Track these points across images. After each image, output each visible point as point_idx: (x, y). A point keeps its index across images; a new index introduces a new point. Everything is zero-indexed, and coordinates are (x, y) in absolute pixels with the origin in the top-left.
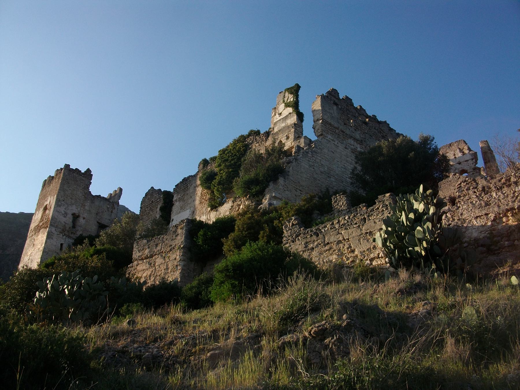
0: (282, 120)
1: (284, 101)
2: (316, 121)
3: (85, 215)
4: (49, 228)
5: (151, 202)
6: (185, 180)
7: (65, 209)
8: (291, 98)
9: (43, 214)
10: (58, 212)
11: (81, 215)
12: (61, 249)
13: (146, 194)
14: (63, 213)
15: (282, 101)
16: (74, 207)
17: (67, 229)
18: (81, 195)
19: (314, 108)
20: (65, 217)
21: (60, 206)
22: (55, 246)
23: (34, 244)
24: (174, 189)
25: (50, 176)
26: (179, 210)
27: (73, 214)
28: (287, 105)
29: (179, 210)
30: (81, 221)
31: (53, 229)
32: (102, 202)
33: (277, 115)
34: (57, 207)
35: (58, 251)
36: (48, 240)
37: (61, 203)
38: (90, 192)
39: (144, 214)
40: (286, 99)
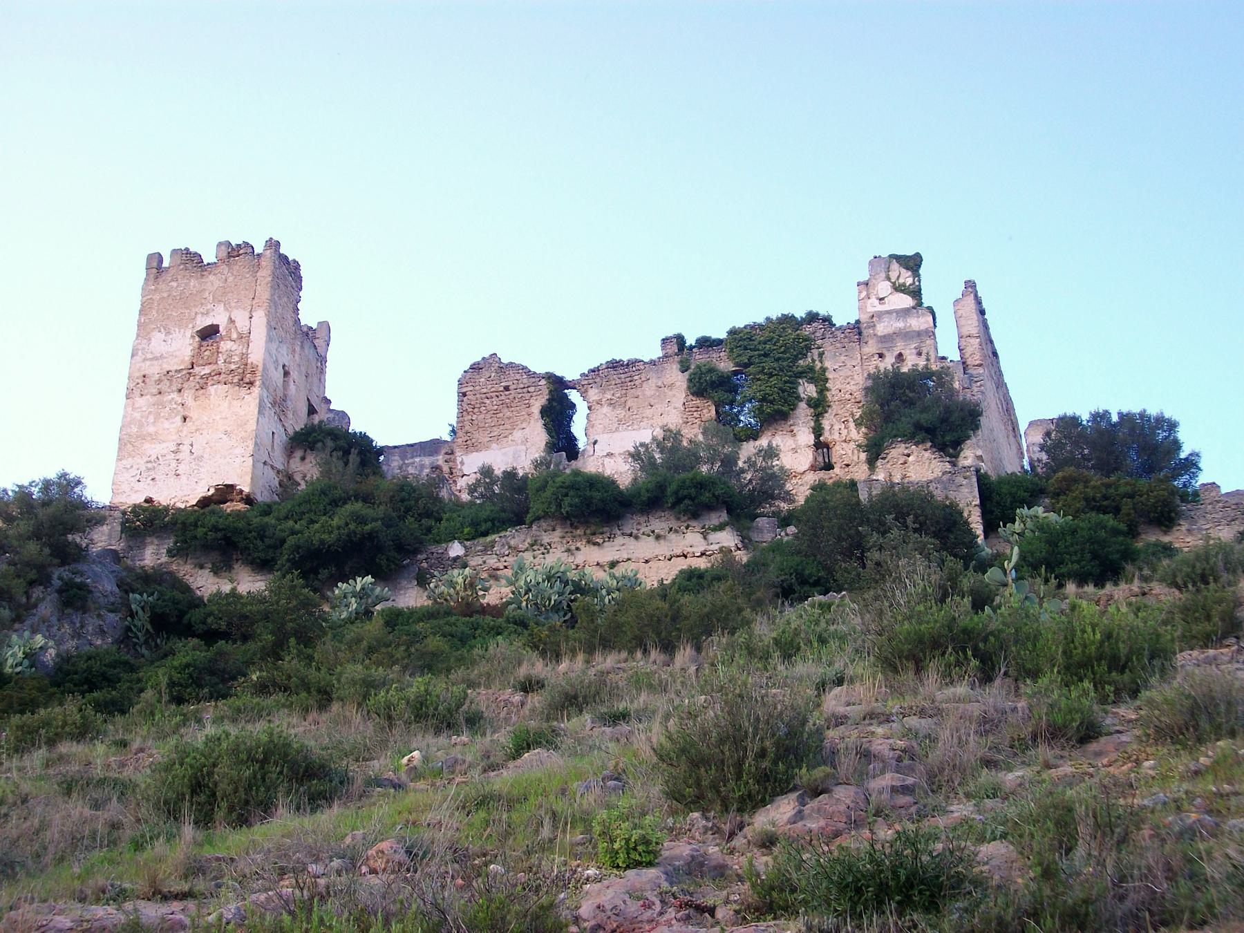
1: (888, 279)
5: (502, 389)
6: (614, 365)
8: (907, 278)
13: (476, 368)
15: (883, 275)
26: (616, 425)
28: (899, 288)
29: (616, 425)
33: (874, 301)
40: (893, 276)
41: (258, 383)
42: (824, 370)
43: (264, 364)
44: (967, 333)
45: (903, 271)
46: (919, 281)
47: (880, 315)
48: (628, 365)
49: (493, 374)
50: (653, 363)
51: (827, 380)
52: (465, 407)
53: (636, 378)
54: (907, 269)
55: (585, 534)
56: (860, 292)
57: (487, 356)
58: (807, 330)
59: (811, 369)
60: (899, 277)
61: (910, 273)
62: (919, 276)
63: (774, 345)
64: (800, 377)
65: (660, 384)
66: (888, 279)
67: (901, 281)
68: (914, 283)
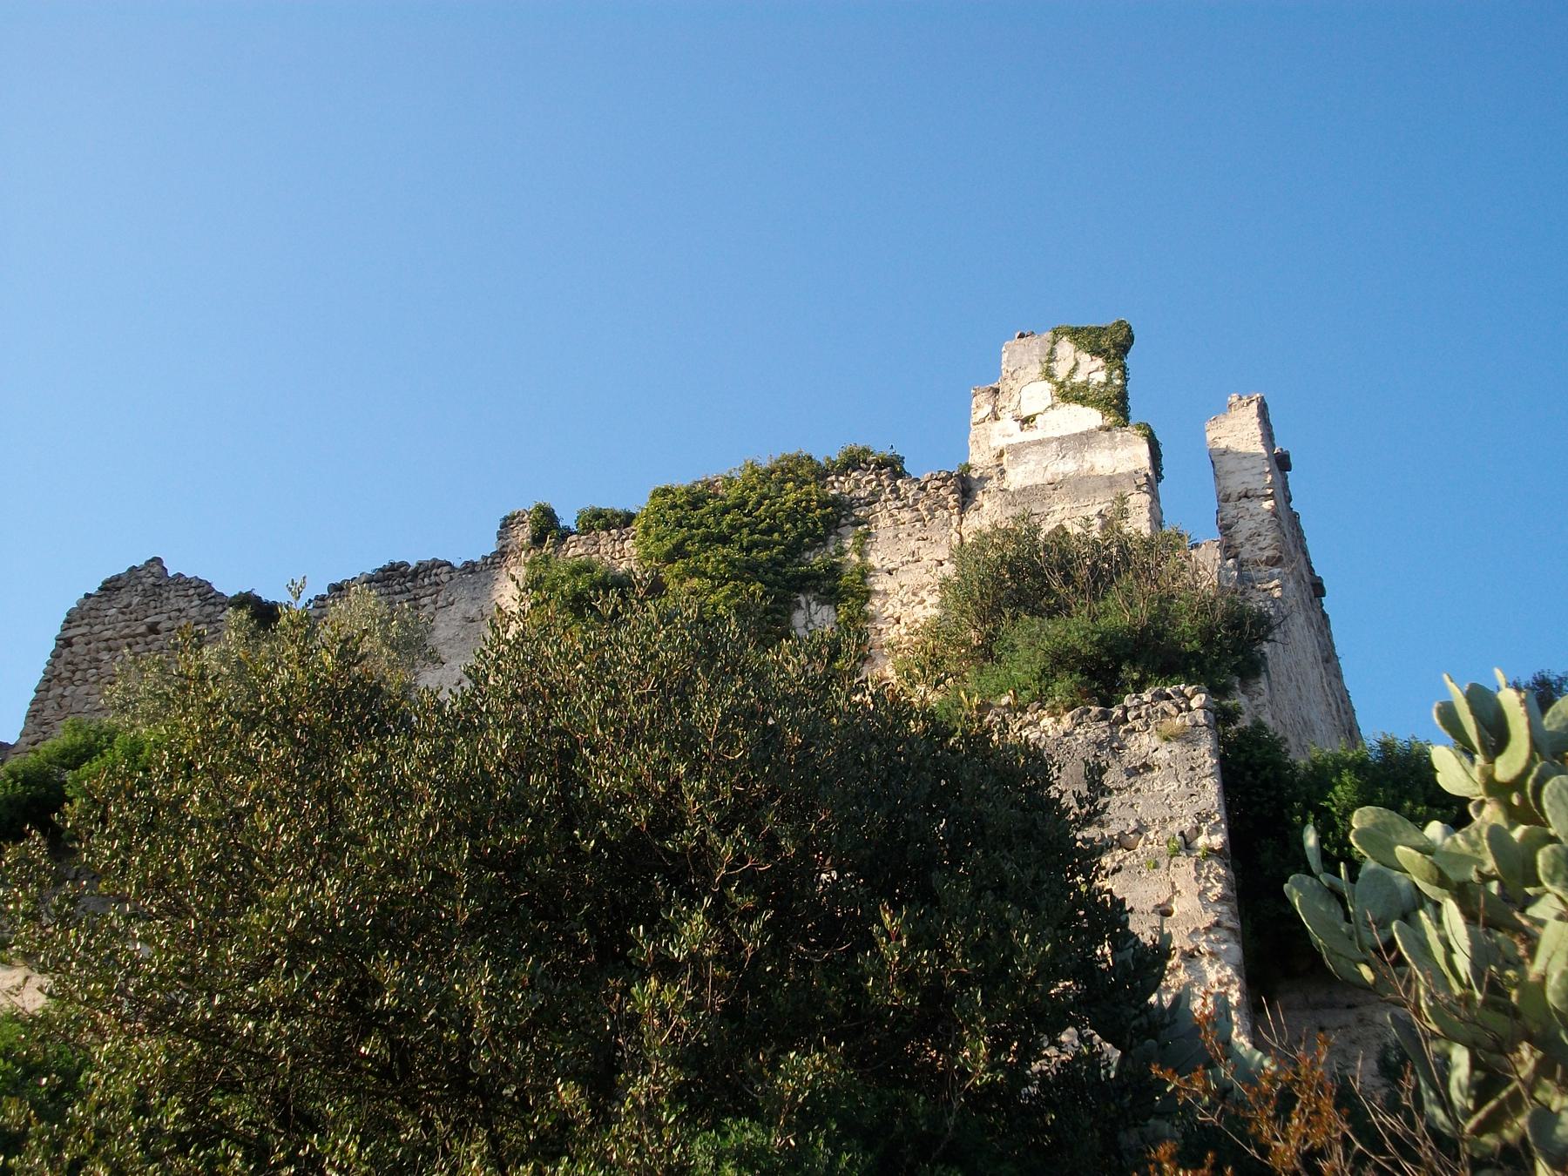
0: (1055, 445)
2: (1235, 496)
5: (142, 629)
8: (1093, 371)
13: (111, 587)
15: (1036, 370)
19: (1222, 445)
24: (88, 596)
25: (157, 561)
28: (1071, 394)
33: (1008, 424)
36: (372, 600)
38: (180, 575)
39: (78, 675)
40: (1061, 371)
42: (865, 572)
44: (1241, 489)
45: (1085, 358)
46: (1124, 376)
47: (1017, 450)
48: (415, 573)
49: (136, 600)
50: (470, 567)
51: (867, 595)
52: (60, 667)
53: (425, 600)
54: (1096, 352)
55: (255, 1089)
57: (140, 563)
58: (840, 486)
59: (834, 571)
60: (1074, 370)
61: (1100, 362)
62: (1124, 370)
63: (749, 514)
64: (800, 590)
65: (473, 612)
66: (1049, 375)
67: (1079, 378)
68: (1109, 381)
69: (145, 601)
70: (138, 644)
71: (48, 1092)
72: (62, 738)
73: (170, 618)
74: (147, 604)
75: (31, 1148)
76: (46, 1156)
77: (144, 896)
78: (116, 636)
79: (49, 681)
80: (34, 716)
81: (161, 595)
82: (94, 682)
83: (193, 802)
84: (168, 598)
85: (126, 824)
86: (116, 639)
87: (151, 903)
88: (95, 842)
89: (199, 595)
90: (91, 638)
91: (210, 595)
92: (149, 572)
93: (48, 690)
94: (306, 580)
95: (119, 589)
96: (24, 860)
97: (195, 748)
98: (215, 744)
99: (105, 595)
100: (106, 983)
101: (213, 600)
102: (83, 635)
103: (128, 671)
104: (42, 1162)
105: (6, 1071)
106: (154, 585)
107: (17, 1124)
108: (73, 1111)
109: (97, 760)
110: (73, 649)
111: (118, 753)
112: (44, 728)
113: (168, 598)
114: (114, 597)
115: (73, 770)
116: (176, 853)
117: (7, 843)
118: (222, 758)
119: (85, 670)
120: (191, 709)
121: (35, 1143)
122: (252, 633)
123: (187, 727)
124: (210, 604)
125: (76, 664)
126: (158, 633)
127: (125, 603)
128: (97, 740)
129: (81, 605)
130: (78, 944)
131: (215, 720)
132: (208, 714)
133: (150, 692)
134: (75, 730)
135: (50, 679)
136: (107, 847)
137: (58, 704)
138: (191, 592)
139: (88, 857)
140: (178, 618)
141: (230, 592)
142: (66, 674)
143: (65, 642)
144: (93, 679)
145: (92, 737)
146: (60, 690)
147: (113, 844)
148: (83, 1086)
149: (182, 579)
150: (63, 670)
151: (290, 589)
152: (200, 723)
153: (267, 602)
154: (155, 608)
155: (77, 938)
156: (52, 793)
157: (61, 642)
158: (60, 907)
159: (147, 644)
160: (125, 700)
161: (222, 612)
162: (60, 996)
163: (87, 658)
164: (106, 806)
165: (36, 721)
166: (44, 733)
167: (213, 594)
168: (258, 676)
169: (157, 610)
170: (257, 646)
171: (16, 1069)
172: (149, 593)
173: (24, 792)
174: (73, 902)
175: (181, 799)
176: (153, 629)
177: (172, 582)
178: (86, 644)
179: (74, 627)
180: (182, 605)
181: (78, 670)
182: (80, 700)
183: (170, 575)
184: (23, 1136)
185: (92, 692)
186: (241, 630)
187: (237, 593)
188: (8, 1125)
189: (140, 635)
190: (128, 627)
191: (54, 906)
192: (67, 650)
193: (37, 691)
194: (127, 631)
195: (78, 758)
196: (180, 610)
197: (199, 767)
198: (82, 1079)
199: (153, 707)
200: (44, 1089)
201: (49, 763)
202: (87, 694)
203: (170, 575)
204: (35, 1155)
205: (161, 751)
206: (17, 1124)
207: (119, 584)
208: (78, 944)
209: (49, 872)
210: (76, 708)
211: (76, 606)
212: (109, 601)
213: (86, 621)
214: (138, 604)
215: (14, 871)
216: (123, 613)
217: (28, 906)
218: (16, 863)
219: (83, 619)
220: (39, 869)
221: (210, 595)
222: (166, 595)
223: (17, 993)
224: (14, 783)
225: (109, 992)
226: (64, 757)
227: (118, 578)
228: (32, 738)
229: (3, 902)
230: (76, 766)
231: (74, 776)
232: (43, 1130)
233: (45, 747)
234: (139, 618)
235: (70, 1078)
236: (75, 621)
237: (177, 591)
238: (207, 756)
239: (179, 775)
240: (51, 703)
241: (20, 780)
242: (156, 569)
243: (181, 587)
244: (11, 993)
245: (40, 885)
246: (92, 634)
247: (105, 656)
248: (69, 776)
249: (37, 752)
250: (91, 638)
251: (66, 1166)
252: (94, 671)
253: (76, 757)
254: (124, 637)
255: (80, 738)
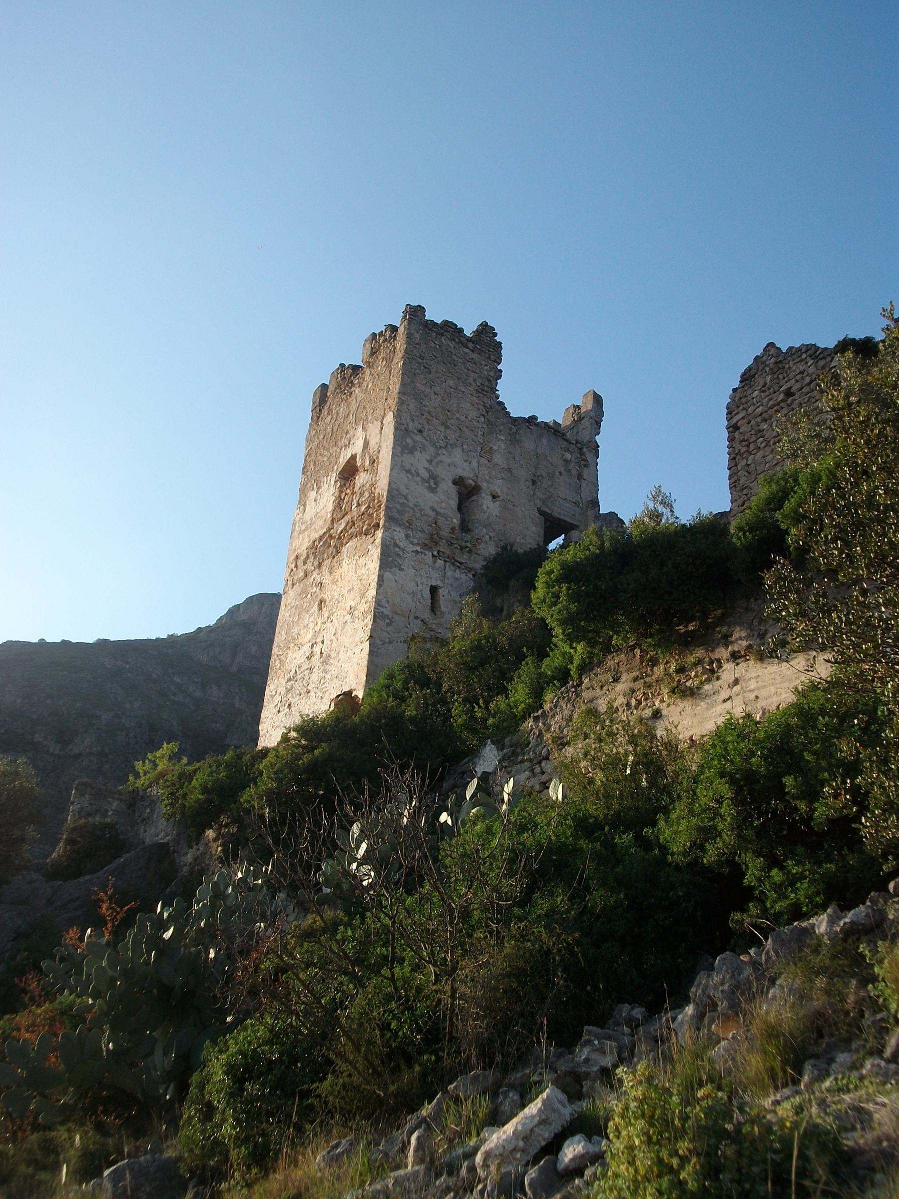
3: (498, 486)
4: (386, 528)
5: (781, 396)
7: (430, 461)
9: (341, 492)
10: (408, 471)
11: (484, 485)
12: (434, 607)
13: (747, 377)
14: (426, 475)
16: (457, 456)
17: (445, 533)
18: (473, 414)
20: (433, 490)
21: (411, 451)
22: (414, 594)
23: (321, 601)
24: (734, 390)
25: (771, 345)
27: (458, 482)
30: (487, 507)
31: (399, 534)
32: (545, 441)
34: (402, 453)
35: (426, 615)
36: (387, 575)
37: (414, 441)
38: (791, 348)
39: (752, 446)
41: (382, 523)
43: (388, 491)
49: (768, 379)
52: (737, 446)
56: (309, 431)
57: (759, 352)
69: (775, 377)
70: (783, 408)
71: (860, 728)
72: (761, 492)
73: (797, 381)
74: (778, 378)
75: (866, 768)
76: (880, 771)
77: (874, 573)
78: (766, 409)
79: (734, 458)
80: (735, 486)
81: (784, 368)
82: (765, 447)
83: (880, 495)
84: (790, 368)
85: (840, 528)
86: (766, 412)
87: (881, 576)
88: (824, 548)
89: (810, 356)
90: (750, 418)
91: (818, 353)
92: (769, 355)
93: (736, 465)
94: (893, 303)
95: (754, 376)
96: (779, 578)
97: (866, 457)
98: (878, 449)
99: (746, 384)
100: (871, 642)
101: (821, 356)
102: (743, 418)
103: (787, 429)
104: (879, 775)
105: (826, 723)
106: (776, 363)
107: (851, 755)
108: (886, 735)
109: (792, 497)
110: (741, 430)
111: (805, 486)
112: (745, 492)
113: (790, 368)
114: (752, 383)
115: (780, 510)
116: (885, 535)
117: (763, 572)
118: (888, 456)
119: (755, 441)
120: (851, 430)
121: (868, 764)
122: (862, 365)
123: (854, 444)
124: (821, 359)
125: (748, 440)
126: (793, 395)
127: (761, 384)
128: (786, 483)
129: (733, 398)
130: (841, 622)
131: (872, 431)
132: (865, 429)
133: (808, 436)
134: (769, 483)
135: (734, 457)
136: (834, 548)
137: (747, 471)
138: (804, 356)
139: (823, 560)
140: (803, 378)
141: (831, 345)
142: (744, 449)
143: (733, 428)
144: (763, 445)
145: (783, 483)
146: (744, 462)
147: (837, 545)
148: (882, 718)
149: (794, 350)
150: (740, 447)
151: (884, 316)
152: (862, 438)
153: (861, 340)
154: (784, 378)
155: (839, 617)
156: (772, 531)
157: (731, 429)
158: (817, 601)
159: (789, 406)
160: (793, 449)
161: (831, 361)
162: (843, 662)
163: (753, 432)
164: (822, 521)
165: (738, 489)
166: (746, 495)
167: (820, 351)
168: (889, 387)
169: (786, 379)
170: (869, 373)
171: (833, 720)
172: (775, 370)
173: (753, 537)
174: (824, 596)
175: (871, 495)
176: (789, 393)
177: (787, 355)
178: (748, 423)
179: (735, 415)
180: (802, 368)
181: (750, 443)
182: (760, 464)
183: (784, 351)
184: (858, 761)
185: (766, 454)
186: (852, 367)
187: (837, 343)
188: (845, 758)
189: (782, 401)
190: (771, 399)
191: (813, 603)
192: (737, 432)
193: (729, 469)
194: (771, 403)
195: (779, 501)
196: (801, 373)
197: (874, 469)
198: (879, 713)
199: (815, 445)
200: (857, 728)
201: (762, 512)
202: (764, 457)
203: (784, 351)
204: (872, 771)
205: (842, 469)
206: (851, 755)
207: (752, 372)
208: (841, 622)
209: (800, 581)
210: (760, 470)
211: (730, 400)
212: (750, 387)
213: (741, 408)
214: (771, 381)
215: (776, 589)
216: (764, 391)
217: (796, 609)
218: (775, 583)
219: (738, 407)
220: (792, 582)
221: (818, 353)
222: (787, 366)
223: (812, 669)
224: (744, 534)
225: (876, 647)
226: (770, 504)
227: (749, 369)
228: (740, 502)
229: (777, 612)
230: (780, 507)
231: (782, 514)
232: (870, 754)
233: (754, 502)
234: (776, 389)
235: (872, 715)
236: (734, 411)
237: (794, 360)
238: (877, 458)
239: (862, 480)
240: (742, 473)
241: (747, 531)
242: (773, 351)
243: (795, 356)
244: (808, 671)
245: (797, 592)
246: (749, 415)
247: (765, 426)
248: (778, 515)
249: (750, 508)
250: (750, 418)
251: (896, 773)
252: (762, 439)
253: (777, 501)
254: (771, 408)
255: (774, 486)
